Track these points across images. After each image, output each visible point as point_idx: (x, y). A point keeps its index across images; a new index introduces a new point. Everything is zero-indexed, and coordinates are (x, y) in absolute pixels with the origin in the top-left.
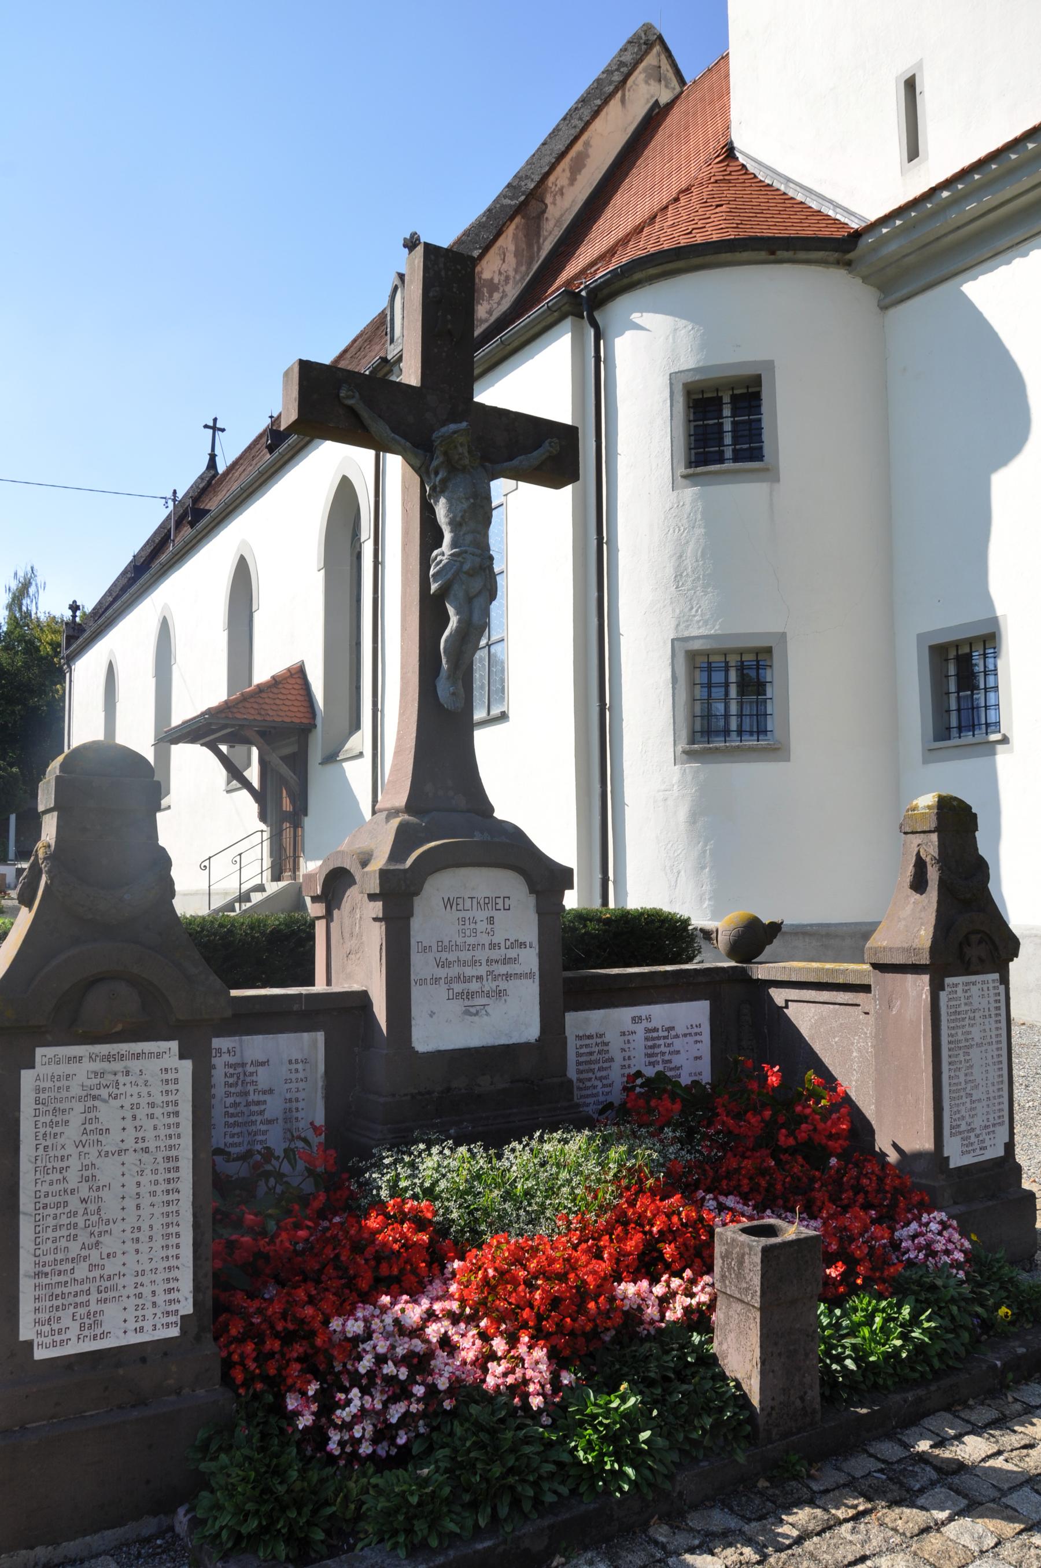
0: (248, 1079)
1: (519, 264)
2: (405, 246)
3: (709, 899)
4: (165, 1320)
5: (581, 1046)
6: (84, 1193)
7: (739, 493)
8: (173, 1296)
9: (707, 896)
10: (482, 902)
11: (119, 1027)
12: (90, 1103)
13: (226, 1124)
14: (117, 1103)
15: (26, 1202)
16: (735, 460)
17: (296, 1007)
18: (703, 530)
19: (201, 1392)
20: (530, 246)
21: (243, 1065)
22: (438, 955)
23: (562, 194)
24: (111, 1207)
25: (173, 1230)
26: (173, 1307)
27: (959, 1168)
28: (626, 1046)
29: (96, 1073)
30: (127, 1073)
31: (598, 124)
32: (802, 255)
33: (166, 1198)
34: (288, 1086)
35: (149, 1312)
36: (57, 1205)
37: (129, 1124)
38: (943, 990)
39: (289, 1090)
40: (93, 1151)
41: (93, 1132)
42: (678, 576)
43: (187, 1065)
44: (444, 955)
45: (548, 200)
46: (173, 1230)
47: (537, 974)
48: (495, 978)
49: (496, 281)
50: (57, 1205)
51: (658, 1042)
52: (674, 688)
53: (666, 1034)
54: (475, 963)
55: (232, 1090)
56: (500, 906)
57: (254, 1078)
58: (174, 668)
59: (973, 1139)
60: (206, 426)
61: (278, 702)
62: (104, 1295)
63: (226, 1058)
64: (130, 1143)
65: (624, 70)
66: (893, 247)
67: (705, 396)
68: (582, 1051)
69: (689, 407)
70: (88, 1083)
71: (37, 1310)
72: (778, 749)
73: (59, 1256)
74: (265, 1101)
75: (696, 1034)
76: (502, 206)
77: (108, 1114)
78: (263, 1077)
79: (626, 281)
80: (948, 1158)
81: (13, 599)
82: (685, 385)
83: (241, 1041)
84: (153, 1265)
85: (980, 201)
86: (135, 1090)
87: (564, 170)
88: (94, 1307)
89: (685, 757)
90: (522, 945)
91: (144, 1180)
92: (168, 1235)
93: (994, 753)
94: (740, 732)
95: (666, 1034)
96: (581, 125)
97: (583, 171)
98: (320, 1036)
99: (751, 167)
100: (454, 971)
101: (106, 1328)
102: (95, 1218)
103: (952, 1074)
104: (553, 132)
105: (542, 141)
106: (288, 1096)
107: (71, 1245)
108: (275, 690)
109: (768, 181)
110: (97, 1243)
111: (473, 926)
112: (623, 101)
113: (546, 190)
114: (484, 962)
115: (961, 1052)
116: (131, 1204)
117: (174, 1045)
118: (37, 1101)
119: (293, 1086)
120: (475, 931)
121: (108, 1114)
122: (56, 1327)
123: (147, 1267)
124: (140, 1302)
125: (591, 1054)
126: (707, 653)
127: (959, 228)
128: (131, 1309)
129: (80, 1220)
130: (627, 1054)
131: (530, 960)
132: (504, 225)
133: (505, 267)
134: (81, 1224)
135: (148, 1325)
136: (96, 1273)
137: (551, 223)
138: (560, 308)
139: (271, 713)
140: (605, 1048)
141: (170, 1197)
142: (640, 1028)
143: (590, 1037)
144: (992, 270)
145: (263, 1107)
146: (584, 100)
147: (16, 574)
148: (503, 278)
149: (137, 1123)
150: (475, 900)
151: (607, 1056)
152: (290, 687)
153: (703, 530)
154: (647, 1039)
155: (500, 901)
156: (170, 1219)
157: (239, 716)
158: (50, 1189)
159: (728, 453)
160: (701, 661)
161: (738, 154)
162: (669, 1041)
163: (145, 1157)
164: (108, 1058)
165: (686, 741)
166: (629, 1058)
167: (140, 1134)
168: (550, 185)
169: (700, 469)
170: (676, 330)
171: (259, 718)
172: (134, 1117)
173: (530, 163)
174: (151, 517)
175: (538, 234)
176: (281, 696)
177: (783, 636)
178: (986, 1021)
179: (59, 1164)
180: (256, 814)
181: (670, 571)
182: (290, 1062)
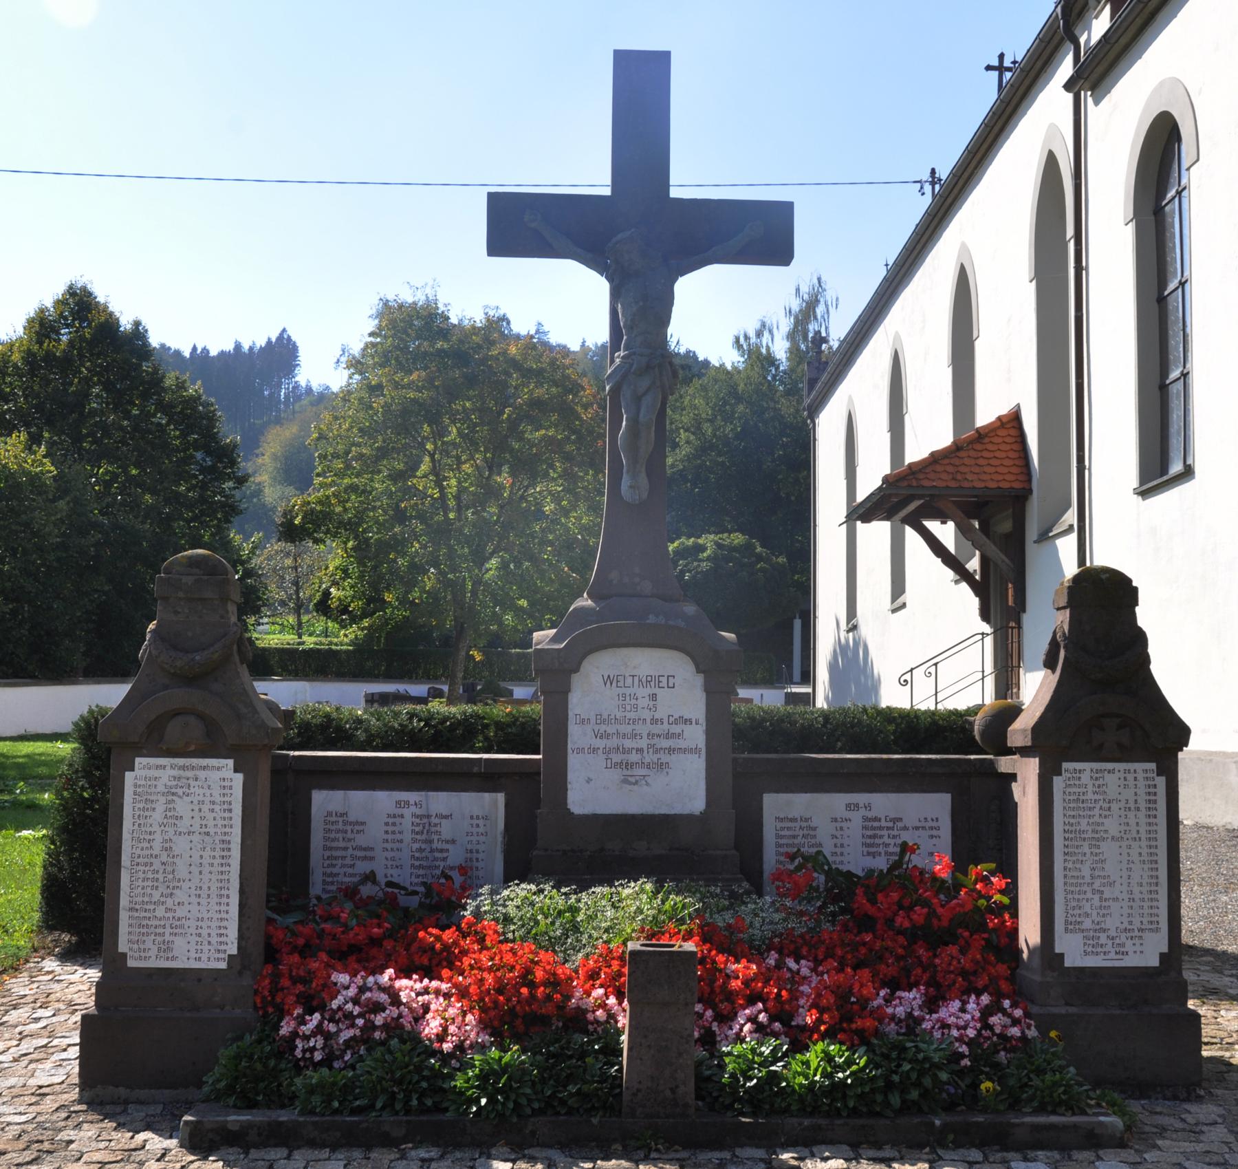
0: (433, 829)
4: (217, 956)
5: (782, 829)
6: (164, 858)
8: (223, 939)
10: (644, 680)
11: (192, 748)
12: (170, 798)
13: (412, 865)
14: (189, 799)
15: (125, 860)
17: (475, 770)
19: (238, 1011)
21: (429, 816)
22: (596, 728)
24: (182, 872)
25: (224, 892)
26: (223, 947)
27: (1075, 968)
28: (838, 834)
29: (175, 778)
30: (196, 779)
33: (220, 869)
34: (469, 838)
35: (206, 947)
36: (146, 864)
37: (196, 814)
38: (1060, 774)
39: (470, 842)
40: (171, 830)
41: (172, 818)
43: (240, 777)
44: (603, 728)
46: (224, 892)
47: (704, 751)
48: (657, 751)
50: (146, 864)
51: (882, 833)
53: (891, 824)
54: (634, 736)
55: (418, 837)
56: (664, 683)
57: (438, 828)
58: (907, 418)
59: (1103, 940)
60: (989, 68)
61: (981, 462)
62: (175, 931)
63: (413, 809)
64: (196, 828)
68: (782, 833)
70: (169, 784)
71: (130, 933)
73: (146, 899)
74: (447, 850)
75: (931, 828)
77: (182, 807)
78: (446, 829)
80: (1062, 955)
83: (427, 796)
84: (210, 915)
86: (201, 791)
88: (167, 937)
90: (688, 721)
91: (206, 854)
92: (221, 896)
95: (891, 824)
98: (501, 797)
100: (613, 742)
101: (175, 953)
102: (171, 876)
103: (1070, 865)
106: (469, 847)
107: (154, 892)
108: (979, 447)
110: (172, 894)
111: (633, 702)
114: (645, 736)
115: (1086, 844)
116: (195, 870)
117: (230, 763)
118: (135, 793)
119: (474, 838)
120: (636, 707)
121: (182, 807)
122: (142, 947)
123: (206, 916)
124: (200, 939)
125: (794, 837)
128: (193, 943)
129: (160, 876)
130: (839, 842)
131: (696, 736)
134: (161, 879)
135: (204, 957)
136: (170, 915)
139: (969, 477)
140: (812, 833)
141: (224, 869)
142: (857, 817)
143: (793, 820)
145: (445, 855)
147: (798, 290)
149: (202, 814)
150: (636, 679)
151: (813, 841)
152: (1000, 440)
154: (865, 828)
155: (664, 680)
156: (224, 884)
157: (926, 483)
158: (142, 853)
162: (895, 832)
163: (207, 838)
164: (183, 768)
167: (204, 823)
171: (953, 484)
172: (200, 810)
176: (985, 454)
178: (1131, 815)
179: (148, 837)
180: (977, 612)
182: (472, 817)
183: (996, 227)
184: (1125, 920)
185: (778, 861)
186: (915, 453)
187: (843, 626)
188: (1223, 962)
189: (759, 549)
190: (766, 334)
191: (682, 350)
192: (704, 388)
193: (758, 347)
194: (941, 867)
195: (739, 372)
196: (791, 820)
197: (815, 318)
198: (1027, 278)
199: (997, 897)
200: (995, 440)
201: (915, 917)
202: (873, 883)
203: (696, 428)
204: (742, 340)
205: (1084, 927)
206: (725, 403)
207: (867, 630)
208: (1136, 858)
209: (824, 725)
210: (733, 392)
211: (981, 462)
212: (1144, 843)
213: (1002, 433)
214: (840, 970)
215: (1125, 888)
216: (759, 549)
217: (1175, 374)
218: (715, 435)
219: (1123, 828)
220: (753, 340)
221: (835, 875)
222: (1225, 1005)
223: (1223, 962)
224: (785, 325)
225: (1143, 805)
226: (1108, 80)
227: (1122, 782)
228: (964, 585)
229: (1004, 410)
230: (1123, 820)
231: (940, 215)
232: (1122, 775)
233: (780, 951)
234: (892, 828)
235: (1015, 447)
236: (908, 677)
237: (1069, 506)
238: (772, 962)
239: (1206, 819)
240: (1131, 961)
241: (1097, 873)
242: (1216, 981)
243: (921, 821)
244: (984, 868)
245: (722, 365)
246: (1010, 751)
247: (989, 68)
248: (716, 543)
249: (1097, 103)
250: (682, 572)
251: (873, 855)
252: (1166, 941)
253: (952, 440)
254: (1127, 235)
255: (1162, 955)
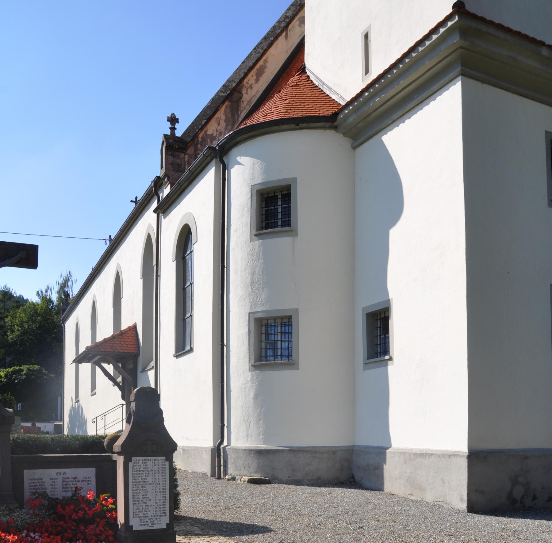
1: (227, 125)
2: (168, 121)
3: (263, 435)
5: (31, 483)
7: (280, 243)
9: (261, 433)
16: (282, 226)
18: (262, 261)
20: (233, 116)
23: (251, 88)
28: (53, 484)
31: (272, 50)
32: (312, 125)
42: (252, 283)
45: (244, 91)
49: (215, 135)
51: (69, 483)
52: (249, 336)
60: (132, 201)
61: (122, 343)
65: (287, 20)
66: (351, 119)
67: (269, 195)
69: (262, 201)
72: (293, 364)
75: (88, 481)
76: (219, 96)
79: (234, 141)
81: (61, 288)
82: (257, 191)
85: (380, 97)
87: (252, 76)
89: (253, 368)
93: (387, 365)
94: (281, 356)
96: (262, 51)
97: (263, 75)
99: (312, 78)
103: (135, 494)
104: (248, 56)
105: (242, 61)
108: (121, 337)
109: (317, 84)
112: (286, 37)
113: (242, 87)
115: (140, 486)
125: (36, 486)
126: (267, 319)
127: (377, 109)
130: (53, 487)
132: (219, 106)
133: (219, 127)
137: (245, 103)
138: (210, 155)
142: (60, 478)
144: (392, 130)
146: (265, 38)
147: (61, 275)
148: (218, 133)
153: (262, 261)
154: (63, 481)
159: (280, 223)
160: (264, 322)
161: (307, 71)
162: (75, 483)
165: (254, 361)
166: (55, 488)
168: (245, 84)
169: (262, 232)
170: (254, 164)
171: (111, 350)
173: (235, 73)
174: (103, 248)
175: (238, 109)
176: (124, 340)
177: (297, 310)
178: (157, 475)
180: (120, 397)
181: (249, 280)
183: (129, 258)
184: (155, 513)
185: (30, 495)
186: (100, 338)
187: (74, 400)
188: (195, 522)
189: (44, 371)
190: (49, 291)
191: (18, 295)
192: (25, 310)
193: (46, 296)
194: (90, 495)
195: (38, 305)
196: (35, 479)
197: (68, 286)
198: (140, 278)
199: (110, 506)
200: (127, 335)
201: (79, 515)
202: (65, 502)
203: (21, 325)
204: (40, 293)
205: (140, 515)
206: (33, 316)
207: (82, 402)
208: (158, 490)
209: (52, 442)
210: (36, 312)
211: (122, 343)
212: (161, 485)
213: (130, 332)
214: (49, 537)
215: (154, 501)
216: (44, 371)
217: (188, 315)
218: (28, 328)
219: (154, 480)
220: (44, 293)
221: (50, 500)
222: (193, 537)
223: (195, 522)
224: (57, 288)
225: (161, 472)
226: (168, 211)
227: (153, 464)
228: (116, 387)
229: (131, 324)
230: (154, 477)
231: (110, 253)
232: (153, 461)
233: (28, 530)
234: (73, 481)
235: (134, 338)
236: (95, 420)
237: (152, 360)
238: (24, 534)
239: (195, 470)
240: (156, 527)
241: (144, 496)
242: (192, 529)
243: (85, 477)
244: (105, 496)
245: (32, 302)
246: (114, 453)
247: (132, 201)
248: (28, 369)
249: (164, 218)
250: (15, 379)
251: (67, 491)
252: (169, 519)
253: (112, 333)
254: (174, 265)
255: (167, 524)
